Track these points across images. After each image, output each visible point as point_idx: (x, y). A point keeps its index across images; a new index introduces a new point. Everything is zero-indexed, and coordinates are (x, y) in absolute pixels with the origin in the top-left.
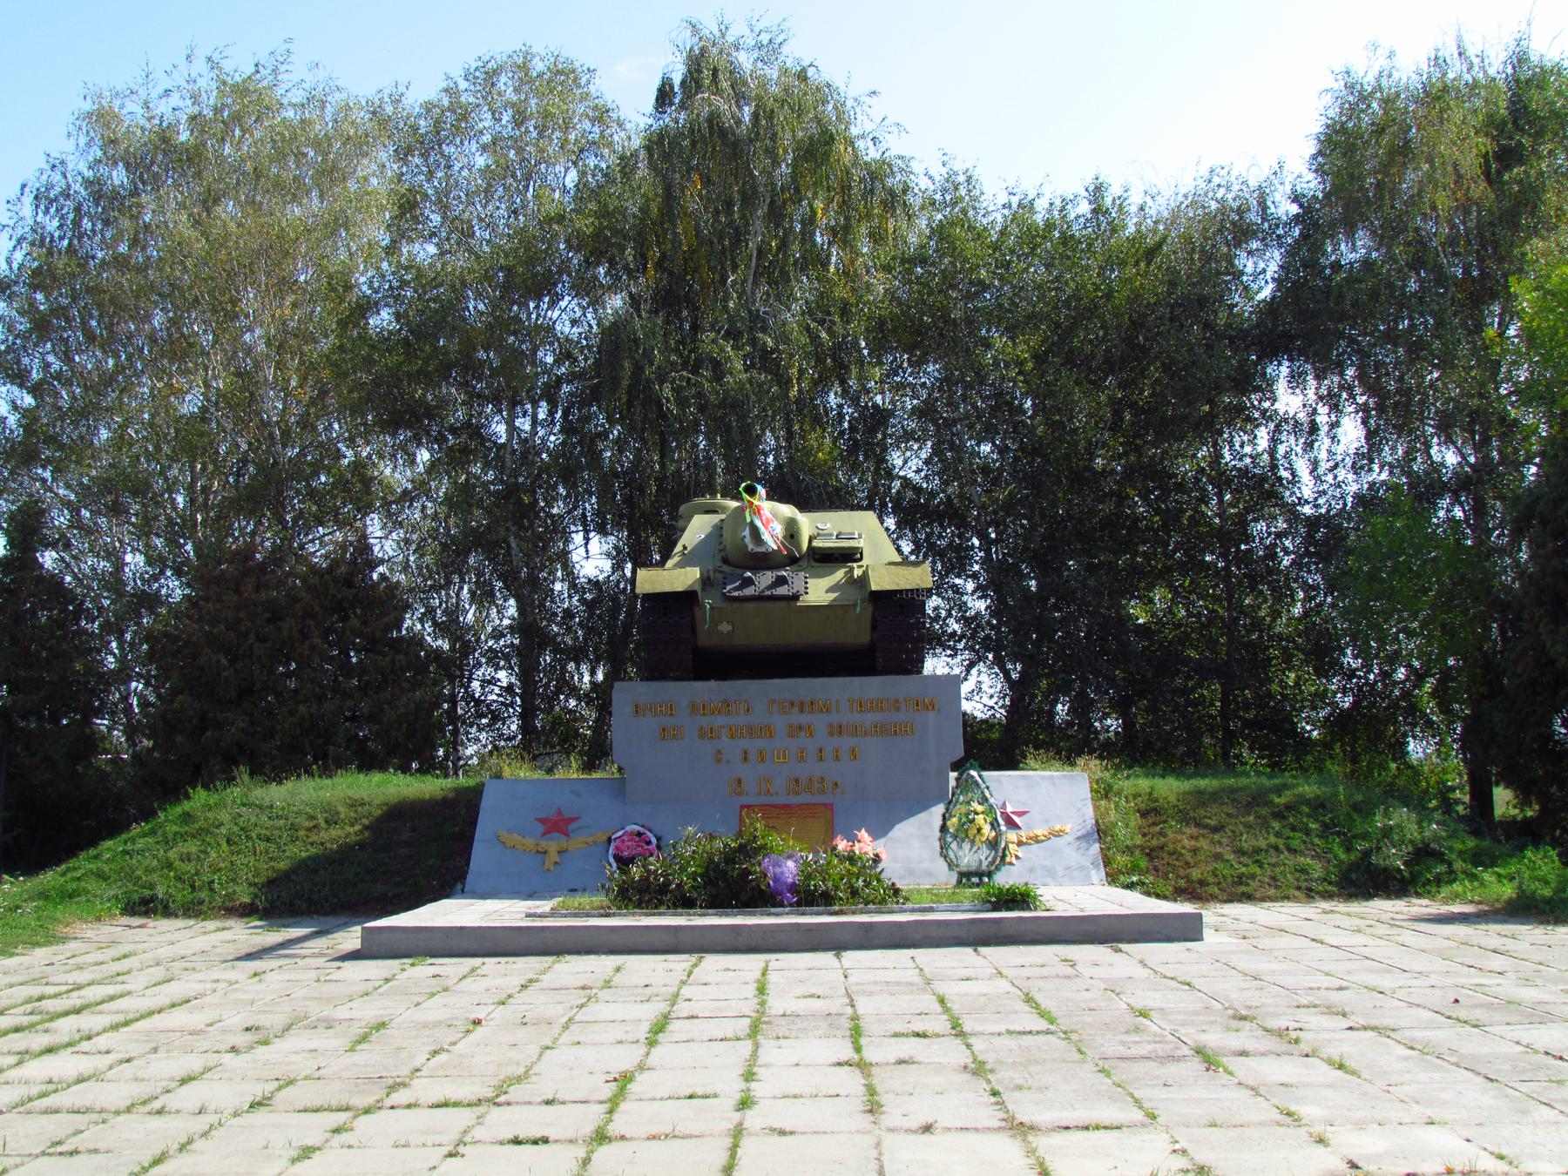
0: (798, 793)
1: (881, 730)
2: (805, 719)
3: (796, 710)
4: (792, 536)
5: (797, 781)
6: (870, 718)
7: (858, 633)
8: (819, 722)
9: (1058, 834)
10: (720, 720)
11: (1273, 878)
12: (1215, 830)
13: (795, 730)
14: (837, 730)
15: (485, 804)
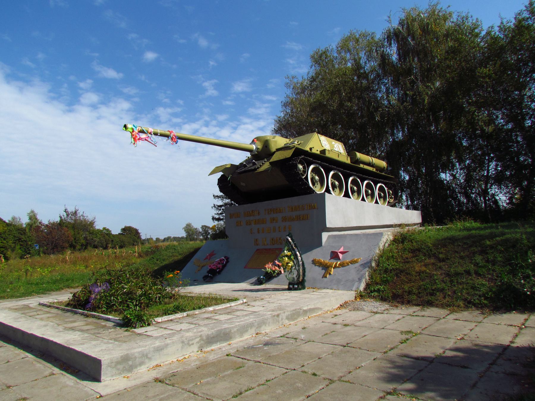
0: (273, 244)
1: (298, 218)
4: (266, 147)
7: (280, 180)
9: (353, 262)
10: (252, 218)
11: (454, 292)
12: (443, 260)
13: (273, 220)
14: (284, 219)
15: (201, 249)
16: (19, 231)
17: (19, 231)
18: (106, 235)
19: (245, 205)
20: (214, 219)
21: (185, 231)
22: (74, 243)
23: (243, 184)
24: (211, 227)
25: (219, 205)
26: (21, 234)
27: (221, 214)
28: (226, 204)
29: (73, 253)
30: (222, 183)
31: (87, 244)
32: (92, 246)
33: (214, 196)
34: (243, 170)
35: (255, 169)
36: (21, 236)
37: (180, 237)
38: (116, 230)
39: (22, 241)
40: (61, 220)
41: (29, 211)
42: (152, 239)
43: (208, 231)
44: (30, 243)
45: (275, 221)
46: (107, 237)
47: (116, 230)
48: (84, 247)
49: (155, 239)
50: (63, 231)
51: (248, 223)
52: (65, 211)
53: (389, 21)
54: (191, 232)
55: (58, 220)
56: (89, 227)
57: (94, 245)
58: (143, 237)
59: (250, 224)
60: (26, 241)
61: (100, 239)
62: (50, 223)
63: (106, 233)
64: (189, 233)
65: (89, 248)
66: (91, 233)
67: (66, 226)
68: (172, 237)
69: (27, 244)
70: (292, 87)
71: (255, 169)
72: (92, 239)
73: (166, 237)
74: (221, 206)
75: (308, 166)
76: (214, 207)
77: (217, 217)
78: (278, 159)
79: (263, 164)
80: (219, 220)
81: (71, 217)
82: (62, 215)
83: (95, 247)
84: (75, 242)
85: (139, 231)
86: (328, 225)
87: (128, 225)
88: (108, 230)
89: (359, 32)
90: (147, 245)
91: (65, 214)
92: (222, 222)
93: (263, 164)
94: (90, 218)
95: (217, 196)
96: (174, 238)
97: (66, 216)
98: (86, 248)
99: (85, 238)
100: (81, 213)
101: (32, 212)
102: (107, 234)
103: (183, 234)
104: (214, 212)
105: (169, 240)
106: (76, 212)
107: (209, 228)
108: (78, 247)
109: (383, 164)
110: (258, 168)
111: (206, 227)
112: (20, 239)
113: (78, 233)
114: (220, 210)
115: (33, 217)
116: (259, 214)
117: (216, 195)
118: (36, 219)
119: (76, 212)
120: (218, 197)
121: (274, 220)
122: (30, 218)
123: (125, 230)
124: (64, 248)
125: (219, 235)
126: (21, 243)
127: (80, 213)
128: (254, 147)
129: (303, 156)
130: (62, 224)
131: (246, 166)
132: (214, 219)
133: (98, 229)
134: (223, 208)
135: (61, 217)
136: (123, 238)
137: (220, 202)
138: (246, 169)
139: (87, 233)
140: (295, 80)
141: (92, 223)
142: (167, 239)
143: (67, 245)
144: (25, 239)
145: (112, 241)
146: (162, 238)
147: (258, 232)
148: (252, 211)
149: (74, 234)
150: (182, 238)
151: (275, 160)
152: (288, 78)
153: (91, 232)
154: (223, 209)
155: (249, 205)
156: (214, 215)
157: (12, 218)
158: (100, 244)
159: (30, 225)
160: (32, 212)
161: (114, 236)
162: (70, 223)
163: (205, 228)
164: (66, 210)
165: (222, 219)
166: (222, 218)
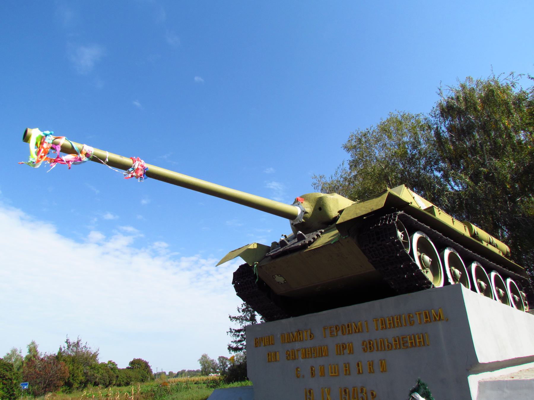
1: (401, 343)
2: (346, 339)
3: (340, 332)
4: (320, 209)
5: (345, 391)
6: (391, 334)
7: (358, 264)
8: (356, 340)
10: (297, 345)
13: (342, 348)
14: (368, 346)
16: (5, 367)
17: (5, 367)
18: (110, 371)
19: (284, 321)
20: (230, 348)
21: (200, 363)
22: (71, 381)
23: (279, 279)
24: (229, 358)
25: (237, 329)
26: (7, 371)
27: (240, 341)
28: (245, 329)
29: (55, 395)
30: (243, 282)
31: (88, 381)
32: (93, 383)
33: (230, 317)
34: (281, 250)
35: (305, 246)
36: (6, 372)
37: (196, 370)
38: (123, 364)
39: (6, 379)
40: (60, 353)
41: (29, 343)
42: (165, 373)
43: (225, 363)
44: (15, 382)
45: (347, 351)
46: (111, 372)
47: (123, 364)
48: (84, 385)
49: (167, 373)
50: (59, 366)
51: (292, 356)
52: (67, 342)
53: (440, 94)
54: (206, 365)
55: (56, 352)
56: (91, 361)
57: (95, 383)
58: (154, 371)
59: (295, 358)
60: (11, 379)
61: (102, 374)
62: (51, 356)
63: (111, 367)
64: (205, 366)
65: (89, 385)
66: (92, 368)
67: (64, 360)
68: (187, 370)
69: (12, 383)
70: (320, 188)
71: (305, 246)
72: (94, 375)
73: (180, 370)
74: (239, 331)
75: (411, 233)
76: (231, 332)
77: (234, 345)
78: (356, 216)
79: (318, 235)
80: (236, 349)
81: (72, 349)
82: (62, 347)
83: (96, 384)
84: (73, 379)
85: (150, 364)
86: (481, 359)
87: (137, 357)
88: (114, 364)
89: (402, 114)
90: (158, 381)
91: (66, 345)
92: (241, 353)
93: (318, 235)
94: (93, 350)
95: (235, 318)
96: (189, 372)
97: (66, 347)
98: (85, 386)
99: (85, 374)
100: (84, 344)
101: (33, 343)
102: (112, 369)
103: (198, 367)
104: (230, 340)
105: (183, 374)
106: (78, 343)
107: (227, 359)
108: (76, 385)
109: (506, 248)
110: (310, 243)
111: (223, 358)
112: (4, 377)
113: (78, 368)
114: (238, 336)
115: (33, 349)
116: (311, 336)
117: (232, 316)
118: (36, 351)
119: (78, 343)
120: (236, 318)
121: (344, 348)
122: (30, 351)
123: (132, 363)
124: (58, 386)
125: (236, 373)
126: (5, 382)
127: (82, 344)
128: (297, 210)
129: (402, 212)
130: (58, 358)
131: (286, 244)
132: (230, 348)
133: (102, 363)
134: (242, 333)
135: (61, 349)
136: (131, 373)
137: (237, 326)
138: (287, 247)
139: (88, 368)
140: (323, 180)
141: (95, 356)
142: (181, 373)
143: (62, 383)
144: (10, 377)
145: (117, 377)
146: (175, 372)
147: (313, 375)
148: (298, 332)
149: (73, 369)
150: (198, 371)
151: (349, 218)
152: (316, 177)
153: (93, 366)
154: (242, 335)
155: (291, 319)
156: (230, 343)
157: (12, 351)
158: (103, 382)
159: (29, 359)
160: (33, 343)
161: (120, 370)
162: (69, 356)
163: (222, 359)
164: (67, 340)
165: (241, 349)
166: (240, 346)
